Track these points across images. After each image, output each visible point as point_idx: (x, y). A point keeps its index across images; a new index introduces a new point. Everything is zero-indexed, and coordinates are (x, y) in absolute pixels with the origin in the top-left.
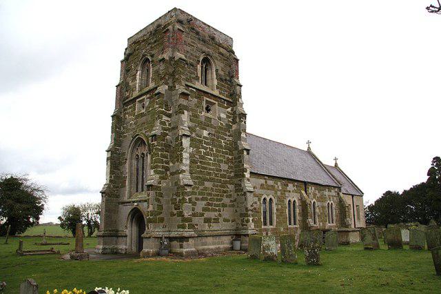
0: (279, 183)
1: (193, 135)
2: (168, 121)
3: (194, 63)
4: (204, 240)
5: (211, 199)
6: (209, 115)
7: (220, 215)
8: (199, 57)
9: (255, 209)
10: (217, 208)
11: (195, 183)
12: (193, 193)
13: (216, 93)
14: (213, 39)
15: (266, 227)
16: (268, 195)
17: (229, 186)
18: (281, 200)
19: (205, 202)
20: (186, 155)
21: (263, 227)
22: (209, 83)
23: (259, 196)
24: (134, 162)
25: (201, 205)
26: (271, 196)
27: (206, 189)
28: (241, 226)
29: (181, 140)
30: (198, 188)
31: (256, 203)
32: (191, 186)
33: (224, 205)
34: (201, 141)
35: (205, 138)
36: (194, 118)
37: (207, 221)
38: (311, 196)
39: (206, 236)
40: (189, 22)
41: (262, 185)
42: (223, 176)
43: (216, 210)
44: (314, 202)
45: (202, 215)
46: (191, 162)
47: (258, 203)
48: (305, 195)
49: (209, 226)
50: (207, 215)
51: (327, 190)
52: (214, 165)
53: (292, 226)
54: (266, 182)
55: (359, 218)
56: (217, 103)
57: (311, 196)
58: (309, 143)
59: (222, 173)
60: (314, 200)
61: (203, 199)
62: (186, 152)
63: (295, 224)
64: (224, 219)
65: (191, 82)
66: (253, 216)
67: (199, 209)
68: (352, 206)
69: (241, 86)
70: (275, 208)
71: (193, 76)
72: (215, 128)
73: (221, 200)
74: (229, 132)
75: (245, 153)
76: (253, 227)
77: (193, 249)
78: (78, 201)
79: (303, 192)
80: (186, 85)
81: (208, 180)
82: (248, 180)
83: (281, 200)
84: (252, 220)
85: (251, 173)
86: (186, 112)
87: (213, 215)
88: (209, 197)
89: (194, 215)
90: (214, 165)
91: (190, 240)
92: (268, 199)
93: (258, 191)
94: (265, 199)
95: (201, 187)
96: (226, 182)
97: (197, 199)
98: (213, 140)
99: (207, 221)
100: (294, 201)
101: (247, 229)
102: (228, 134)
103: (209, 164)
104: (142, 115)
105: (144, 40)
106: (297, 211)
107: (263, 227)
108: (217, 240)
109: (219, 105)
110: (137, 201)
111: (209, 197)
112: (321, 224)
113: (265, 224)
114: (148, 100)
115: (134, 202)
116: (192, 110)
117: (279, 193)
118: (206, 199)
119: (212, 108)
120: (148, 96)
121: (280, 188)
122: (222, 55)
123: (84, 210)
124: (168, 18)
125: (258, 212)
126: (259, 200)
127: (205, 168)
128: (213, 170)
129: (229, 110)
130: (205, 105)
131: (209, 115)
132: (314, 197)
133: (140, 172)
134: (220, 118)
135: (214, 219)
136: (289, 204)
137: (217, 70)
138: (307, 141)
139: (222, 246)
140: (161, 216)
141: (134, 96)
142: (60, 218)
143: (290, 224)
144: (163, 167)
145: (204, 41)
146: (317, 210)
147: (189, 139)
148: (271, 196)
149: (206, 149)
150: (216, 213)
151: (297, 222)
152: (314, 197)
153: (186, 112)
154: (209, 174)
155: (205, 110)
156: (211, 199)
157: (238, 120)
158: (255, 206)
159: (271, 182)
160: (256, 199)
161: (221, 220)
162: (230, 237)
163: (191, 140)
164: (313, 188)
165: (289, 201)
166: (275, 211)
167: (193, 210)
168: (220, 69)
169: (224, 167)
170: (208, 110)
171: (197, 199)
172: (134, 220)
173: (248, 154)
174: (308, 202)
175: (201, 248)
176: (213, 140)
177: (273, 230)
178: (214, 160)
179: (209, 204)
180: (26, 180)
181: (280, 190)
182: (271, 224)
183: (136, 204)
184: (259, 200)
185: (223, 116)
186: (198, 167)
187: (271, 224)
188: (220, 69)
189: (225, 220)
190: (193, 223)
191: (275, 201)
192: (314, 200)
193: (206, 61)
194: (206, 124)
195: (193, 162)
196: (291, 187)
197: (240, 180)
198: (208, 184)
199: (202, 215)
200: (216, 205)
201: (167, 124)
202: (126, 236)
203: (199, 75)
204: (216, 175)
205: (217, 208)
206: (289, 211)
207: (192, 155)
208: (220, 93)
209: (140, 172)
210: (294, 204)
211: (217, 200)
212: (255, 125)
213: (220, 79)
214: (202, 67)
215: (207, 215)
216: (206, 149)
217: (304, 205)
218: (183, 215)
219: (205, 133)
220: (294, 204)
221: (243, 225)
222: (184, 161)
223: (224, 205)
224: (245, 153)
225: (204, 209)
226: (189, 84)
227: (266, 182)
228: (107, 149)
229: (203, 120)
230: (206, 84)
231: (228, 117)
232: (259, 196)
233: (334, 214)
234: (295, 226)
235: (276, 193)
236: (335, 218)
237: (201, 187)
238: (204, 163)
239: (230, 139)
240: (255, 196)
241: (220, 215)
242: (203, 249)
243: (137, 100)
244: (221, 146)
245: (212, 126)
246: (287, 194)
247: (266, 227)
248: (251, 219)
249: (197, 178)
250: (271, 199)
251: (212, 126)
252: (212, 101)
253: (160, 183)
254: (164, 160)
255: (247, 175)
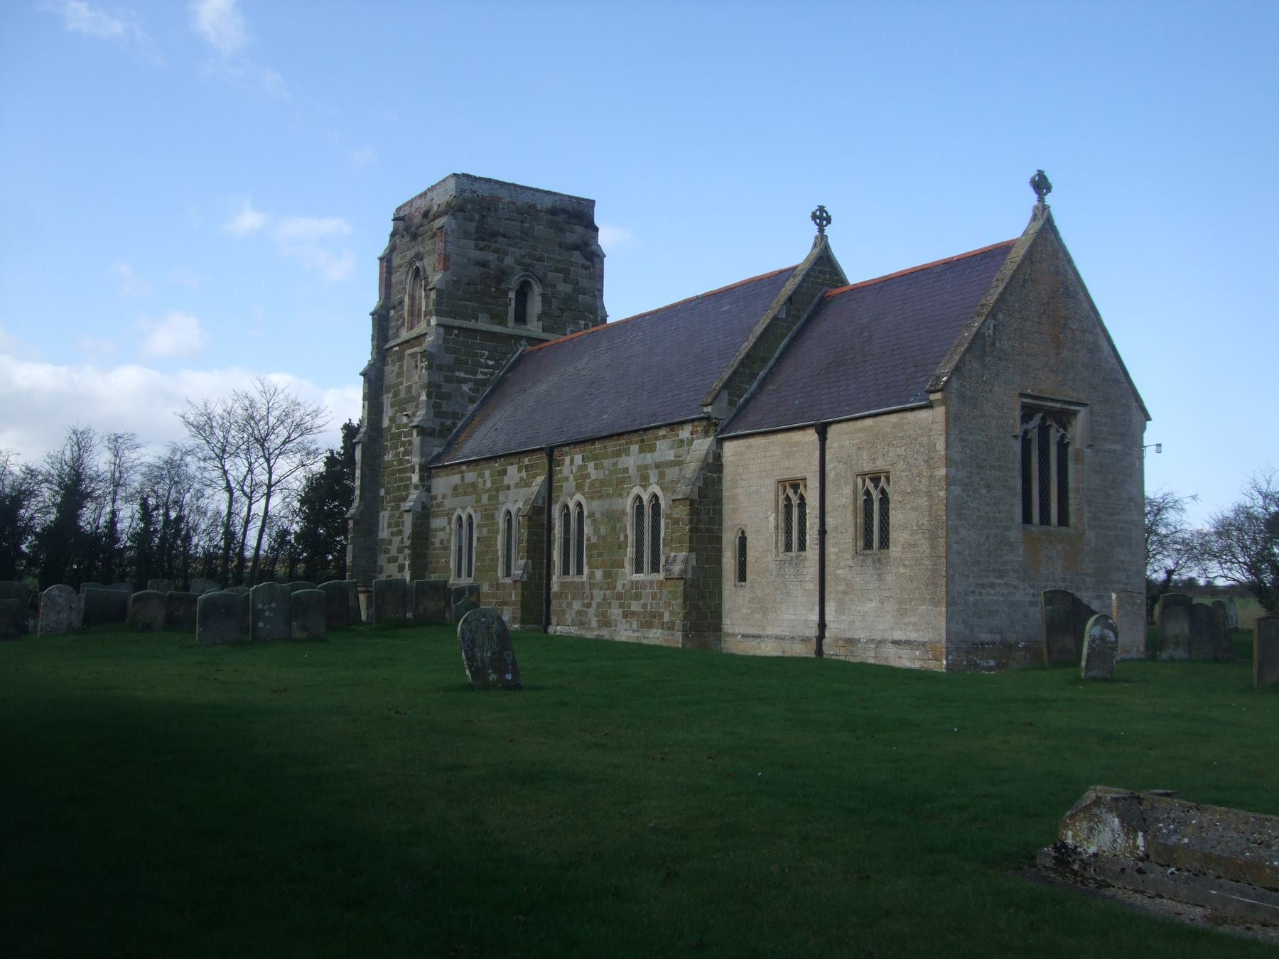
16: (464, 508)
21: (628, 574)
26: (470, 510)
41: (455, 488)
58: (350, 420)
78: (815, 234)
92: (464, 518)
117: (485, 498)
123: (1091, 829)
132: (579, 488)
148: (470, 510)
152: (579, 488)
180: (1176, 505)
192: (579, 497)
212: (1147, 494)
228: (361, 370)
234: (577, 579)
235: (478, 500)
250: (470, 517)
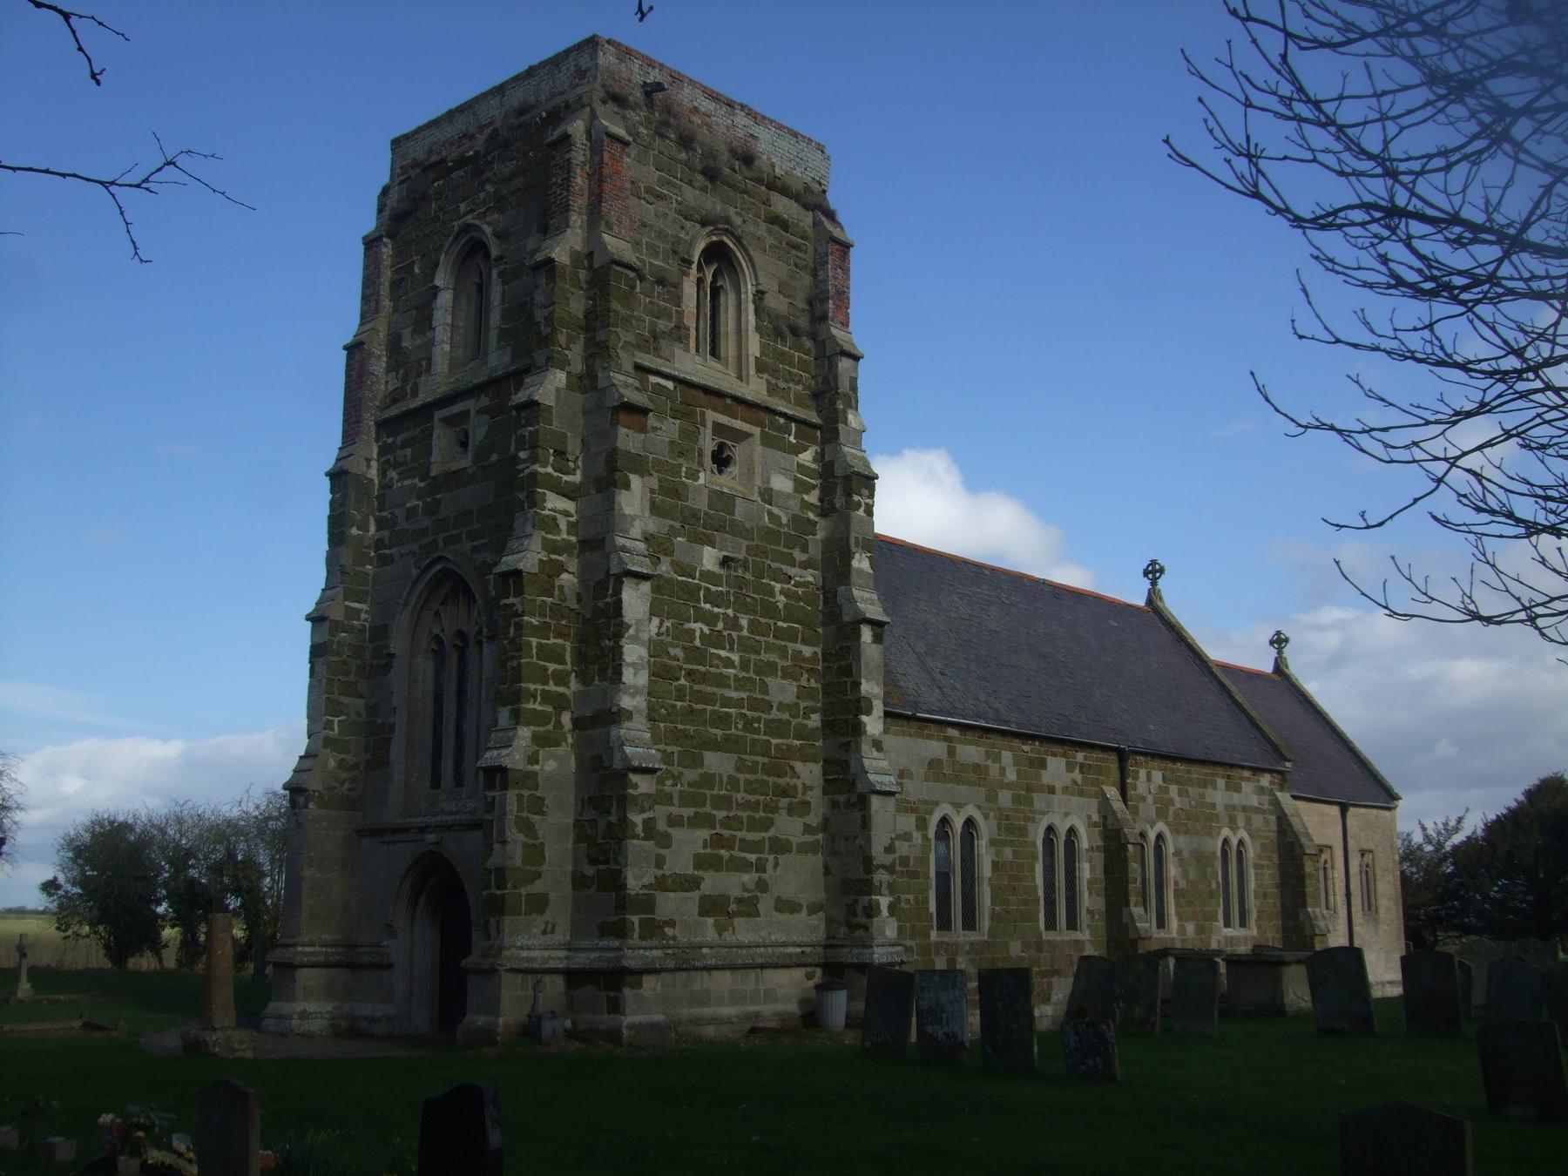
0: (1007, 756)
1: (665, 568)
2: (566, 514)
3: (671, 267)
4: (702, 982)
5: (726, 823)
6: (727, 482)
7: (762, 886)
8: (691, 244)
9: (904, 861)
10: (752, 857)
11: (667, 757)
12: (663, 798)
13: (755, 388)
14: (748, 159)
15: (946, 938)
16: (958, 806)
17: (798, 766)
18: (1012, 829)
19: (704, 834)
20: (633, 652)
21: (934, 935)
22: (729, 346)
23: (920, 812)
24: (426, 667)
25: (688, 844)
26: (971, 810)
27: (708, 780)
28: (843, 931)
29: (618, 592)
30: (677, 778)
31: (907, 837)
32: (652, 771)
33: (780, 846)
34: (691, 593)
35: (708, 576)
36: (668, 500)
37: (713, 906)
38: (1148, 808)
39: (708, 969)
40: (648, 94)
41: (934, 764)
42: (778, 728)
43: (744, 866)
44: (1160, 837)
45: (694, 884)
46: (653, 674)
47: (917, 837)
48: (1118, 805)
49: (720, 930)
50: (712, 882)
51: (1221, 782)
52: (741, 684)
53: (1062, 935)
54: (951, 752)
55: (1370, 907)
56: (756, 431)
57: (1148, 808)
59: (775, 714)
60: (1161, 826)
61: (697, 822)
62: (635, 639)
63: (1072, 924)
64: (779, 899)
65: (657, 351)
66: (892, 888)
67: (680, 860)
68: (1339, 853)
69: (856, 358)
70: (985, 859)
71: (663, 325)
72: (747, 534)
73: (766, 825)
74: (805, 550)
75: (866, 634)
76: (891, 931)
77: (659, 1017)
79: (1112, 792)
80: (639, 368)
81: (716, 746)
82: (878, 745)
83: (1012, 829)
84: (892, 908)
85: (887, 714)
86: (635, 481)
87: (732, 884)
88: (720, 815)
89: (661, 884)
90: (741, 684)
91: (649, 982)
92: (958, 823)
93: (915, 789)
94: (944, 821)
95: (691, 775)
96: (787, 753)
97: (674, 821)
98: (740, 584)
99: (713, 906)
100: (1072, 831)
101: (866, 945)
102: (799, 556)
103: (721, 681)
104: (453, 479)
105: (462, 162)
106: (1085, 871)
107: (934, 935)
108: (749, 982)
109: (767, 441)
110: (437, 828)
111: (720, 815)
112: (1190, 928)
113: (945, 923)
114: (485, 418)
115: (423, 829)
116: (659, 465)
117: (1005, 798)
118: (708, 821)
119: (737, 451)
120: (484, 401)
121: (1011, 776)
122: (784, 225)
124: (564, 77)
125: (913, 875)
126: (922, 824)
127: (709, 699)
128: (738, 703)
129: (807, 457)
130: (708, 443)
131: (727, 482)
132: (1161, 814)
133: (450, 708)
134: (768, 495)
135: (740, 901)
136: (1049, 843)
137: (760, 295)
138: (1270, 634)
139: (767, 1009)
140: (538, 886)
141: (423, 398)
142: (50, 887)
143: (1051, 924)
144: (547, 697)
145: (711, 174)
146: (1172, 871)
147: (646, 587)
148: (1243, 834)
149: (710, 619)
150: (748, 878)
151: (1084, 918)
152: (1161, 814)
153: (635, 481)
154: (724, 721)
155: (708, 461)
156: (726, 823)
157: (839, 502)
158: (903, 848)
159: (971, 752)
160: (907, 823)
161: (765, 903)
162: (799, 973)
163: (656, 589)
164: (1157, 776)
165: (1050, 829)
166: (986, 870)
167: (660, 862)
168: (770, 286)
169: (782, 690)
170: (721, 460)
171: (674, 821)
172: (423, 898)
173: (877, 639)
174: (1131, 833)
175: (685, 1012)
176: (740, 584)
177: (975, 947)
178: (744, 665)
179: (718, 841)
181: (1009, 786)
182: (1243, 924)
183: (431, 837)
184: (922, 824)
185: (782, 484)
186: (681, 694)
187: (970, 922)
188: (770, 286)
189: (786, 906)
190: (660, 915)
191: (986, 829)
192: (1161, 826)
193: (717, 254)
194: (702, 528)
195: (661, 673)
196: (1056, 769)
197: (846, 747)
198: (717, 763)
199: (694, 884)
200: (747, 846)
201: (563, 525)
202: (390, 966)
203: (690, 322)
204: (749, 724)
205: (752, 857)
206: (1049, 870)
207: (656, 649)
208: (772, 390)
209: (450, 708)
210: (1240, 855)
211: (753, 825)
213: (773, 327)
214: (700, 282)
215: (712, 882)
216: (710, 619)
217: (1114, 844)
218: (623, 887)
219: (709, 558)
220: (1240, 855)
221: (853, 927)
222: (628, 676)
223: (780, 846)
224: (866, 634)
225: (701, 862)
226: (648, 360)
227: (951, 752)
229: (701, 504)
230: (715, 353)
231: (801, 487)
232: (920, 812)
233: (1252, 885)
235: (992, 797)
236: (1253, 904)
237: (691, 775)
238: (704, 678)
239: (810, 576)
240: (906, 808)
241: (762, 886)
242: (698, 1021)
243: (438, 414)
244: (770, 610)
245: (736, 530)
246: (1039, 801)
247: (946, 938)
248: (884, 902)
249: (677, 737)
250: (970, 823)
251: (736, 530)
252: (738, 424)
253: (533, 759)
254: (552, 667)
255: (873, 724)
